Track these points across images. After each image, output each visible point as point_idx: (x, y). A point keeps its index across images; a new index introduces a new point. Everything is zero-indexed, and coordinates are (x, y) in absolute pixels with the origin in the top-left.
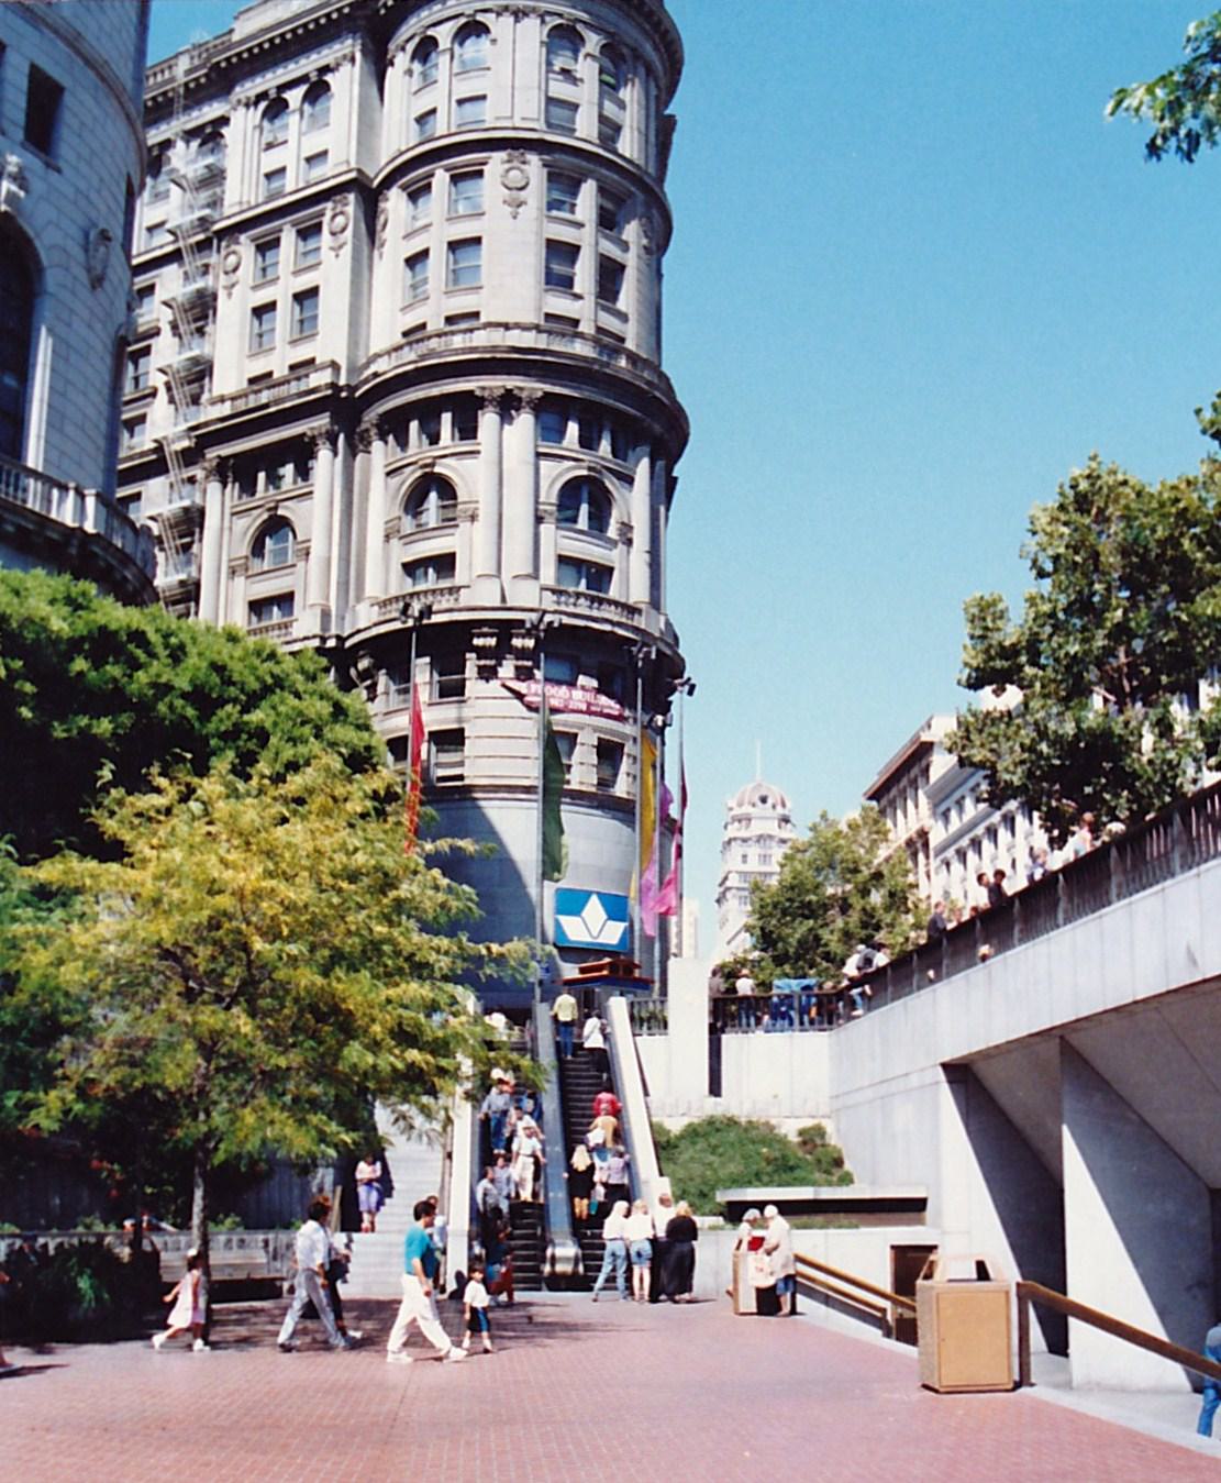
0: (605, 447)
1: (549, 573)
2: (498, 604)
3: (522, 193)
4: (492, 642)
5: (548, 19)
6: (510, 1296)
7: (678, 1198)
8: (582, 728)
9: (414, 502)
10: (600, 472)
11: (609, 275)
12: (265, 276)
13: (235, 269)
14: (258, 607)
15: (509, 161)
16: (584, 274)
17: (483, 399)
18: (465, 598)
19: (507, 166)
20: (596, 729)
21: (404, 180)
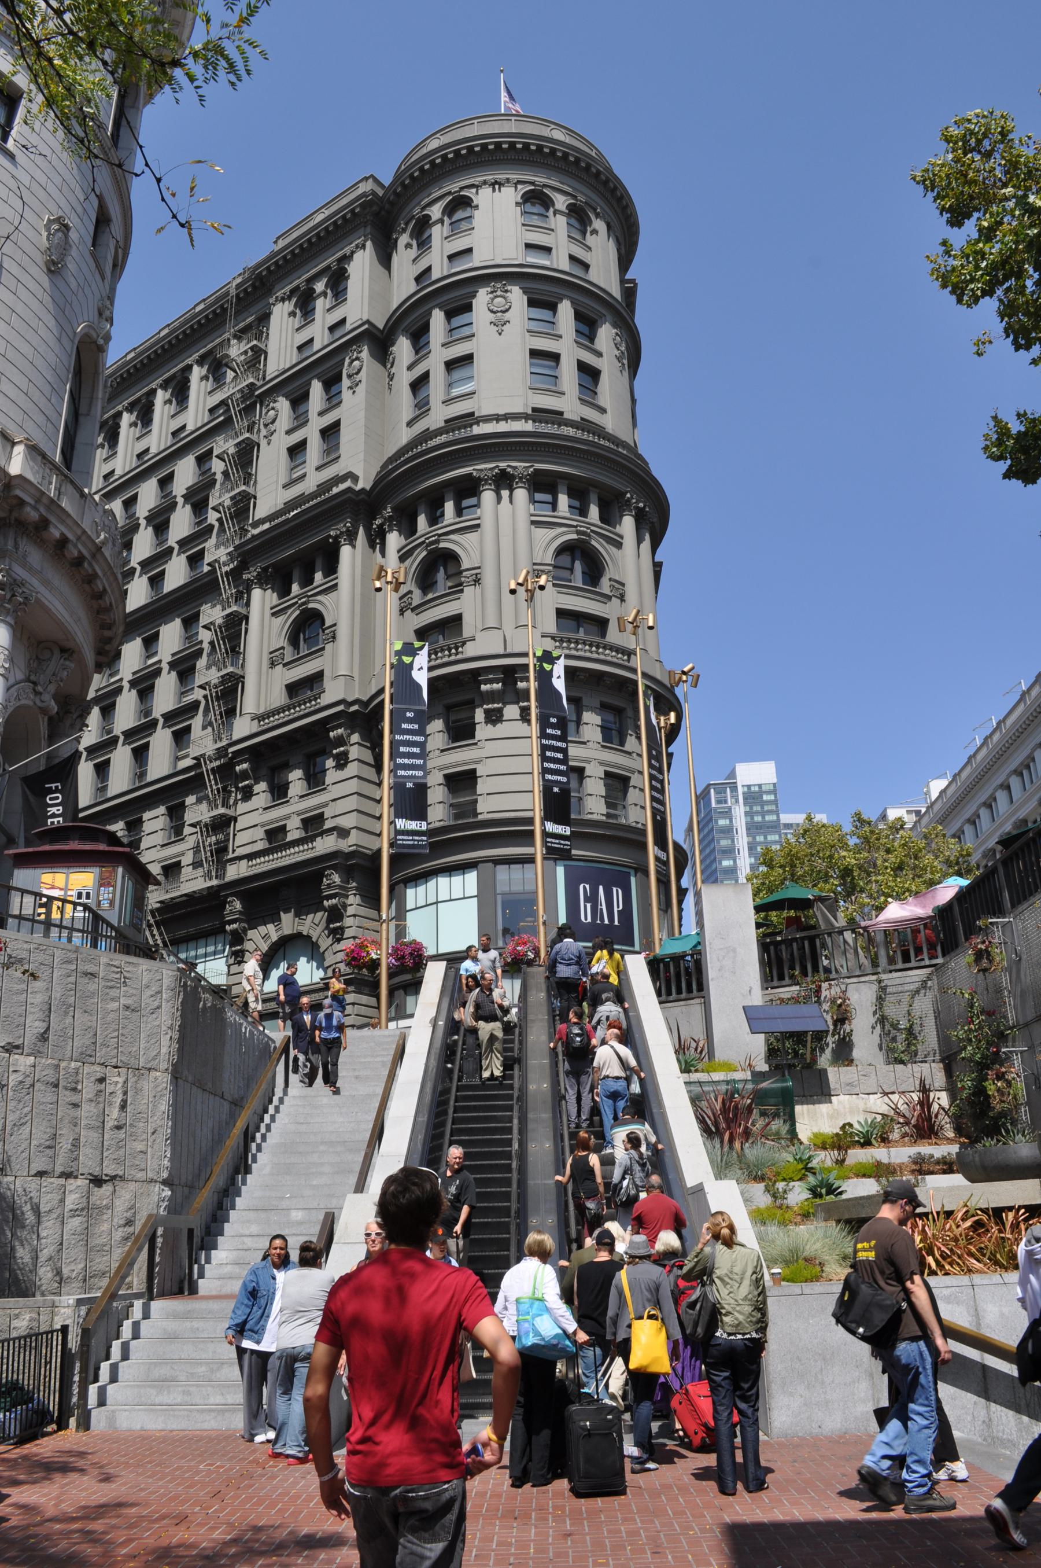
0: (594, 511)
1: (550, 624)
2: (501, 651)
3: (507, 314)
4: (498, 686)
5: (519, 187)
6: (765, 838)
7: (170, 80)
8: (589, 762)
9: (425, 579)
10: (589, 536)
11: (589, 374)
12: (300, 421)
13: (273, 422)
14: (293, 689)
15: (492, 292)
16: (568, 375)
17: (479, 479)
18: (470, 651)
19: (491, 296)
20: (602, 763)
21: (406, 324)
